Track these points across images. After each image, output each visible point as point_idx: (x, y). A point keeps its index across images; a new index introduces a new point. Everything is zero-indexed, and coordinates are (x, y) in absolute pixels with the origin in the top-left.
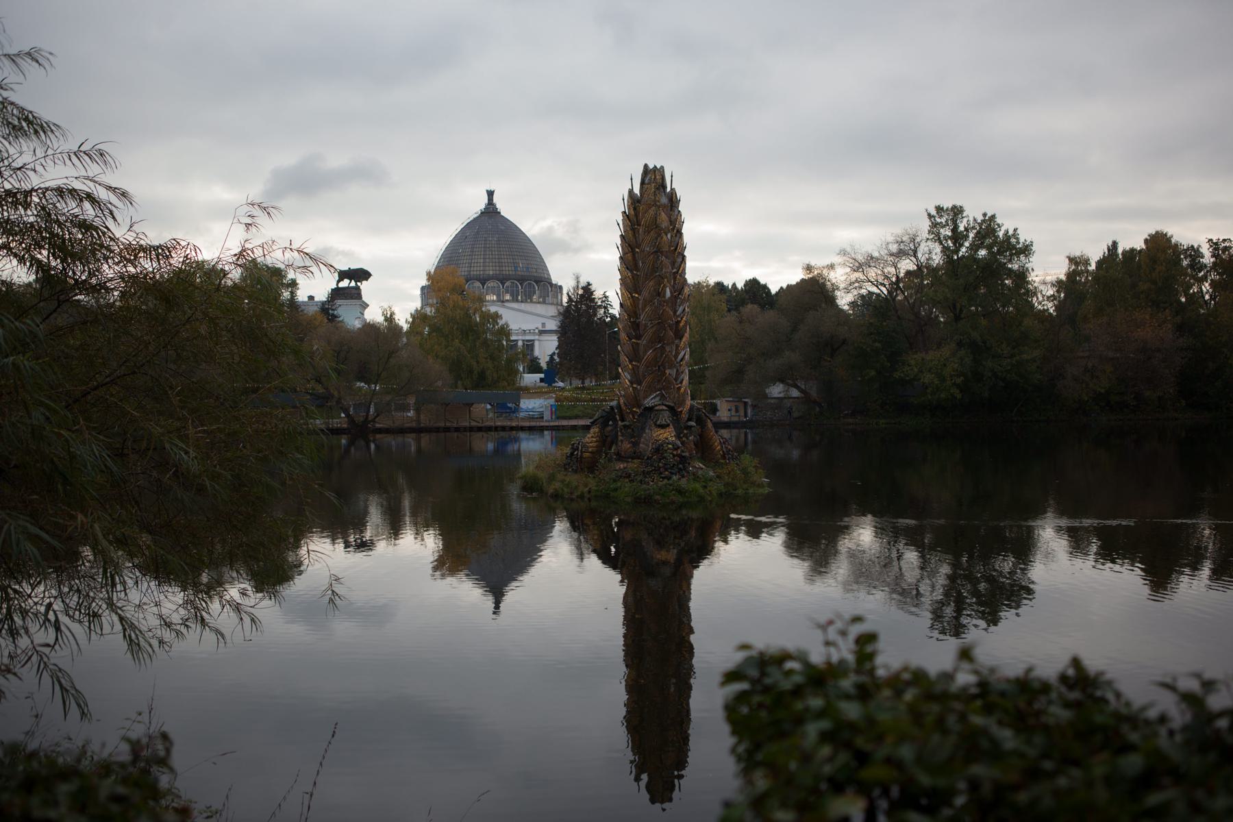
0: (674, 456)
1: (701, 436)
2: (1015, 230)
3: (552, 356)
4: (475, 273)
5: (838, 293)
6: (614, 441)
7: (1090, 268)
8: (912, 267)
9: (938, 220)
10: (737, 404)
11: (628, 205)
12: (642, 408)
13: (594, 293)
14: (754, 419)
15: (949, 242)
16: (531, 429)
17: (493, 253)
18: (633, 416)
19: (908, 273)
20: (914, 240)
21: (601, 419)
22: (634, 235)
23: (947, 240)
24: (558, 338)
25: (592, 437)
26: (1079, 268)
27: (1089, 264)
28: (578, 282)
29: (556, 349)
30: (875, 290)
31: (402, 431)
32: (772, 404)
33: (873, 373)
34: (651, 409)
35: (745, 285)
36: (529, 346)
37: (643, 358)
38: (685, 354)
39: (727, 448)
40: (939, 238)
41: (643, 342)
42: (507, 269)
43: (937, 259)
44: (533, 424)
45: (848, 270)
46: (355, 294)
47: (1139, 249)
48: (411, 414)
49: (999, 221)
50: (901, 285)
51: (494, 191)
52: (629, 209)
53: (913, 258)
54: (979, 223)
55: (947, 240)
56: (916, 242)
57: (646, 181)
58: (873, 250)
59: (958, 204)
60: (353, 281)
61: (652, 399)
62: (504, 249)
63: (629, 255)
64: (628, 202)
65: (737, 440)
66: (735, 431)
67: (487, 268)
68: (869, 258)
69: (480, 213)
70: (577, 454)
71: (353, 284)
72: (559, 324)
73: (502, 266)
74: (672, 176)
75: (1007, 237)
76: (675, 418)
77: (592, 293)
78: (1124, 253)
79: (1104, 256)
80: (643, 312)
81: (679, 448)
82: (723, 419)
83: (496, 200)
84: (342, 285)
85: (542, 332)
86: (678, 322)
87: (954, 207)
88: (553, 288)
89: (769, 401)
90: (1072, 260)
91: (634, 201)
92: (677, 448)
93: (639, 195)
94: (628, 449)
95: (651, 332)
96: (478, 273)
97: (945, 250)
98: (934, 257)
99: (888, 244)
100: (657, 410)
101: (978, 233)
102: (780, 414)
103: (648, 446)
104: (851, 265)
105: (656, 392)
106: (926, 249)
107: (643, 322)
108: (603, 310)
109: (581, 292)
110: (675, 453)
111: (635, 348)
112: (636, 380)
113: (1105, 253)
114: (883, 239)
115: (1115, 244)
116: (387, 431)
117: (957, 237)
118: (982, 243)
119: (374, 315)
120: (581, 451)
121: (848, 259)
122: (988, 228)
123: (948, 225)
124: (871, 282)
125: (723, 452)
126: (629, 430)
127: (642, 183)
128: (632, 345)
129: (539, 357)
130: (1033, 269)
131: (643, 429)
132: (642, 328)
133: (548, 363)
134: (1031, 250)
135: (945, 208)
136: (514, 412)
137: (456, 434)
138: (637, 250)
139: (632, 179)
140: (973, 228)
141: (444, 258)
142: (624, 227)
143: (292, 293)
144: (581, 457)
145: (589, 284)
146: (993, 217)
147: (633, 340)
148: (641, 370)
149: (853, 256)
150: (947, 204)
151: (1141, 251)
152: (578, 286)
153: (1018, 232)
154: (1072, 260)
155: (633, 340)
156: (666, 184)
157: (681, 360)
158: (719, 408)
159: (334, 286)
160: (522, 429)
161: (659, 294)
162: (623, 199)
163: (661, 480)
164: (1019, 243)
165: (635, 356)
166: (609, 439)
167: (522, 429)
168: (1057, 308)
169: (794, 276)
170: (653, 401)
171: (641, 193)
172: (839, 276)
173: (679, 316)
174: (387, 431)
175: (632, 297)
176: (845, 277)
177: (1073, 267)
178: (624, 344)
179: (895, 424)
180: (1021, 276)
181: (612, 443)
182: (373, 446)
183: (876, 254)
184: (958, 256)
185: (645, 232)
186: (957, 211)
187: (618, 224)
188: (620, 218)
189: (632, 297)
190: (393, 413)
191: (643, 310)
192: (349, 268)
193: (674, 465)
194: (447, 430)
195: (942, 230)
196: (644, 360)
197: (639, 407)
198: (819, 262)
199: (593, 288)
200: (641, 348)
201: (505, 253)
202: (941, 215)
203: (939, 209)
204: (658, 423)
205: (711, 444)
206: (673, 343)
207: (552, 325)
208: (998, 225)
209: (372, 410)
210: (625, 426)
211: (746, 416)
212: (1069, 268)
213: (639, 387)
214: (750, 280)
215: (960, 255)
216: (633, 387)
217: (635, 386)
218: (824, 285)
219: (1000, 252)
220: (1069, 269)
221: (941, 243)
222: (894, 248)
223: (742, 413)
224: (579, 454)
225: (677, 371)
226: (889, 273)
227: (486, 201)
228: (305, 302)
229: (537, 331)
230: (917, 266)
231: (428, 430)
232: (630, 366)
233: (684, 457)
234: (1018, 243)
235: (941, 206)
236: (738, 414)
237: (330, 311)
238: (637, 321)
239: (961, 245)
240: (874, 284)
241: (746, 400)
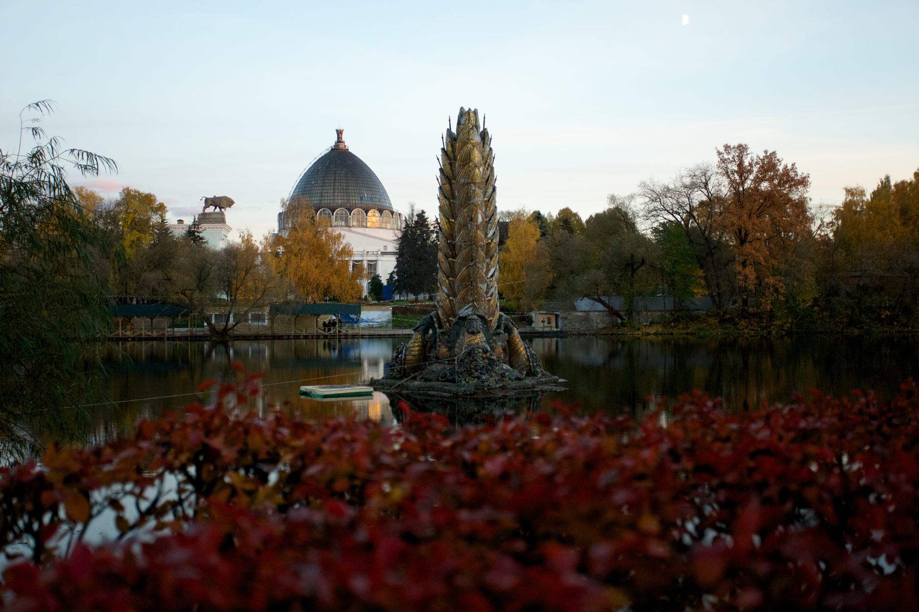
0: (483, 358)
1: (508, 341)
2: (793, 165)
3: (391, 274)
4: (326, 202)
5: (638, 220)
6: (433, 346)
7: (865, 199)
8: (705, 198)
9: (726, 156)
10: (549, 316)
11: (446, 143)
12: (457, 317)
13: (427, 220)
14: (564, 329)
15: (736, 175)
16: (371, 337)
17: (342, 185)
18: (450, 324)
19: (702, 203)
20: (705, 174)
21: (422, 327)
22: (451, 168)
23: (733, 174)
24: (397, 258)
25: (415, 342)
26: (855, 198)
27: (864, 194)
28: (413, 210)
29: (395, 268)
30: (672, 219)
31: (257, 338)
32: (579, 316)
33: (13, 191)
34: (464, 319)
35: (559, 214)
36: (373, 265)
37: (458, 275)
38: (494, 272)
39: (530, 352)
40: (727, 172)
41: (458, 260)
42: (354, 198)
43: (725, 190)
44: (372, 332)
45: (647, 199)
46: (221, 220)
47: (909, 181)
48: (266, 323)
49: (779, 156)
50: (695, 214)
51: (343, 130)
52: (447, 146)
53: (704, 190)
54: (761, 159)
55: (733, 174)
56: (707, 176)
57: (462, 122)
58: (669, 183)
59: (743, 143)
60: (218, 207)
61: (466, 309)
62: (351, 181)
63: (447, 185)
64: (447, 140)
65: (550, 347)
66: (547, 340)
67: (336, 198)
68: (666, 190)
69: (330, 149)
70: (401, 357)
71: (218, 210)
72: (397, 246)
73: (350, 196)
74: (484, 118)
75: (786, 172)
76: (485, 326)
77: (425, 220)
78: (896, 185)
79: (878, 188)
80: (458, 235)
81: (487, 351)
82: (536, 329)
83: (344, 138)
84: (207, 210)
85: (383, 254)
86: (488, 244)
87: (740, 146)
88: (394, 216)
89: (577, 313)
90: (849, 191)
91: (452, 139)
92: (485, 351)
93: (456, 134)
94: (445, 353)
95: (464, 252)
96: (329, 201)
97: (732, 182)
98: (723, 189)
99: (682, 177)
100: (470, 319)
101: (762, 167)
102: (587, 325)
103: (461, 350)
104: (650, 196)
105: (469, 303)
106: (716, 182)
107: (459, 243)
108: (435, 235)
109: (416, 218)
110: (484, 356)
111: (452, 266)
112: (453, 293)
113: (879, 185)
114: (678, 173)
115: (888, 178)
116: (245, 338)
117: (742, 171)
118: (765, 176)
119: (234, 238)
120: (405, 354)
121: (648, 191)
122: (769, 164)
123: (735, 161)
124: (667, 211)
125: (528, 356)
126: (447, 337)
127: (459, 124)
128: (449, 263)
129: (380, 275)
130: (810, 199)
131: (458, 335)
132: (457, 248)
133: (388, 281)
134: (808, 181)
135: (732, 146)
136: (356, 322)
137: (304, 341)
138: (454, 181)
139: (450, 120)
140: (757, 163)
141: (299, 189)
142: (443, 162)
143: (162, 216)
144: (405, 359)
145: (423, 212)
146: (774, 153)
147: (450, 259)
148: (456, 284)
149: (652, 188)
150: (734, 143)
151: (911, 183)
152: (412, 214)
153: (796, 166)
154: (849, 191)
155: (450, 259)
156: (479, 125)
157: (492, 276)
158: (534, 320)
159: (201, 211)
160: (363, 336)
161: (471, 220)
162: (443, 138)
163: (472, 379)
164: (797, 175)
165: (451, 273)
166: (429, 344)
167: (363, 336)
168: (836, 233)
169: (602, 206)
170: (466, 311)
171: (457, 132)
172: (638, 206)
173: (490, 238)
174: (245, 338)
175: (449, 222)
176: (644, 206)
177: (850, 198)
178: (442, 262)
179: (686, 334)
180: (801, 206)
181: (431, 347)
182: (231, 352)
183: (671, 186)
184: (743, 188)
185: (460, 166)
186: (742, 149)
187: (438, 159)
188: (440, 154)
189: (449, 222)
190: (250, 322)
191: (459, 233)
192: (214, 196)
193: (483, 367)
194: (297, 337)
195: (729, 166)
196: (458, 276)
197: (454, 316)
198: (622, 193)
199: (426, 215)
200: (457, 266)
201: (352, 185)
202: (729, 152)
203: (727, 147)
204: (470, 331)
205: (517, 349)
206: (484, 261)
207: (392, 247)
208: (778, 160)
209: (231, 319)
210: (442, 333)
211: (557, 327)
212: (846, 198)
213: (454, 299)
214: (564, 209)
215: (745, 187)
216: (450, 300)
217: (451, 298)
218: (626, 214)
219: (779, 184)
220: (846, 200)
221: (729, 177)
222: (688, 181)
223: (554, 324)
224: (403, 357)
225: (488, 285)
226: (683, 202)
227: (336, 139)
228: (175, 225)
229: (379, 253)
230: (708, 196)
231: (280, 338)
232: (447, 281)
233: (492, 360)
234: (796, 175)
235: (729, 145)
236: (550, 325)
237: (196, 234)
238: (454, 242)
239: (746, 179)
240: (670, 213)
241: (558, 313)
